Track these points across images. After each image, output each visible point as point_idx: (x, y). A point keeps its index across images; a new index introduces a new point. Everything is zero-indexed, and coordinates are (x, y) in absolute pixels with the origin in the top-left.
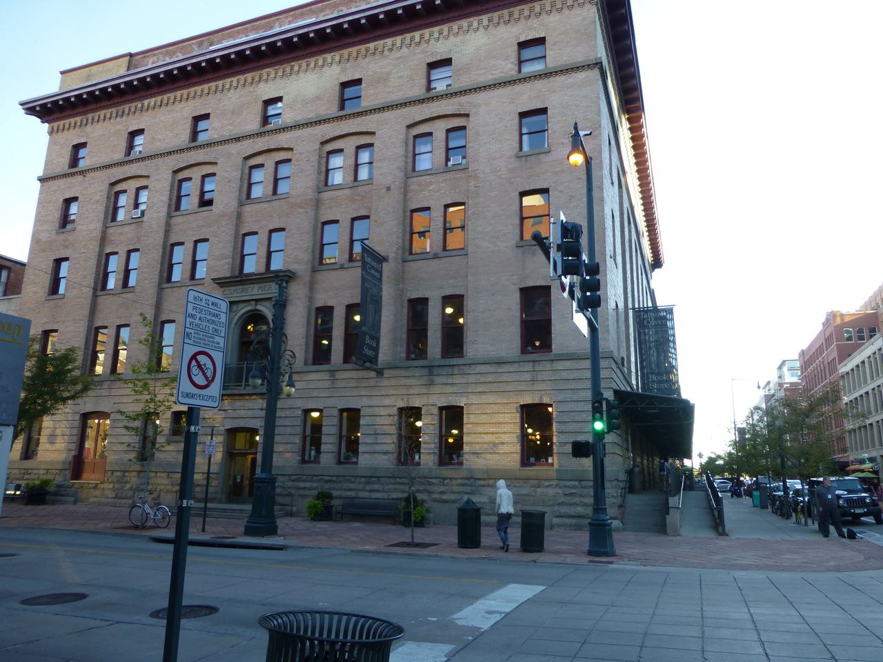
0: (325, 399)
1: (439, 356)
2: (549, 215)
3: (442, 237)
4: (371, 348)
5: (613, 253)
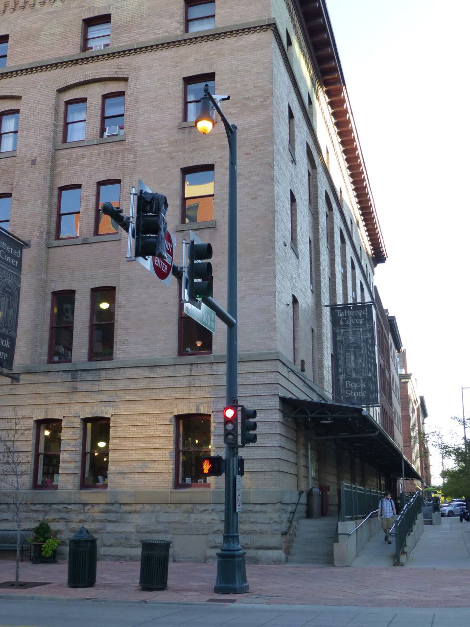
1: (85, 359)
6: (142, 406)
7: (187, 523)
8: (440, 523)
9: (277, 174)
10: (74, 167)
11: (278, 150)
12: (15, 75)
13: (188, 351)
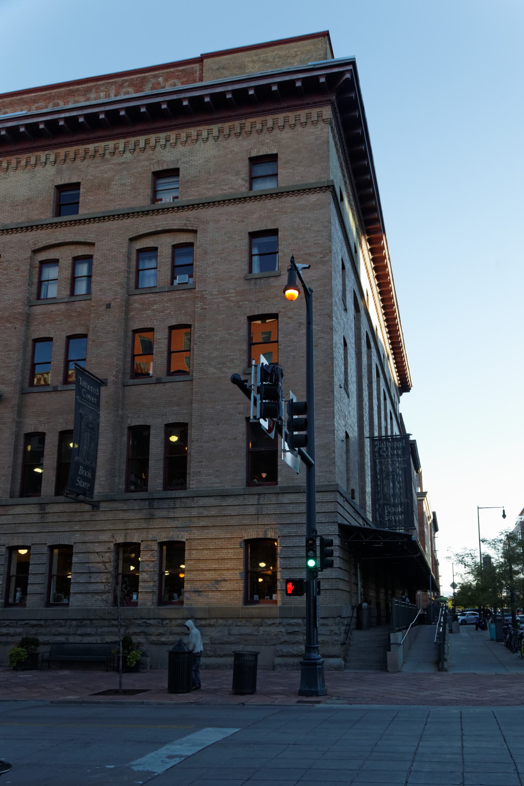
0: (33, 535)
1: (160, 488)
2: (277, 342)
3: (165, 362)
4: (84, 479)
5: (343, 382)
6: (214, 531)
7: (256, 635)
8: (458, 632)
9: (335, 324)
10: (147, 312)
11: (335, 302)
12: (88, 222)
13: (255, 482)
